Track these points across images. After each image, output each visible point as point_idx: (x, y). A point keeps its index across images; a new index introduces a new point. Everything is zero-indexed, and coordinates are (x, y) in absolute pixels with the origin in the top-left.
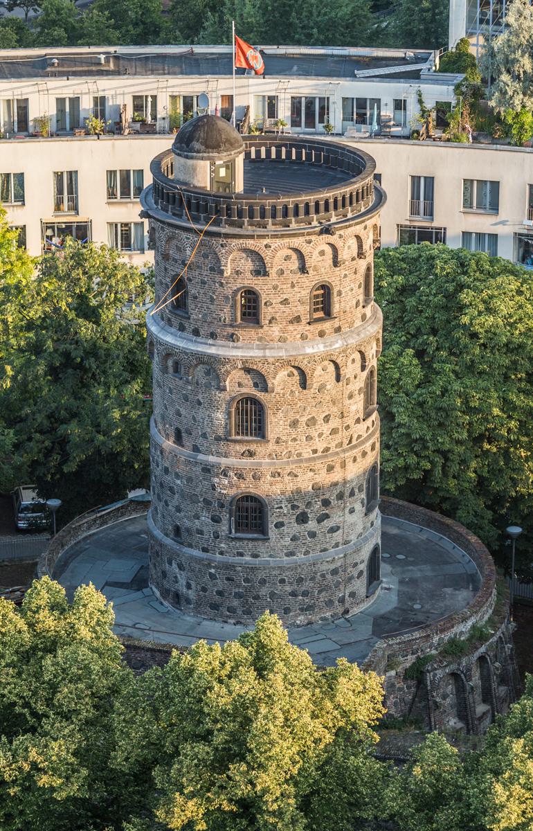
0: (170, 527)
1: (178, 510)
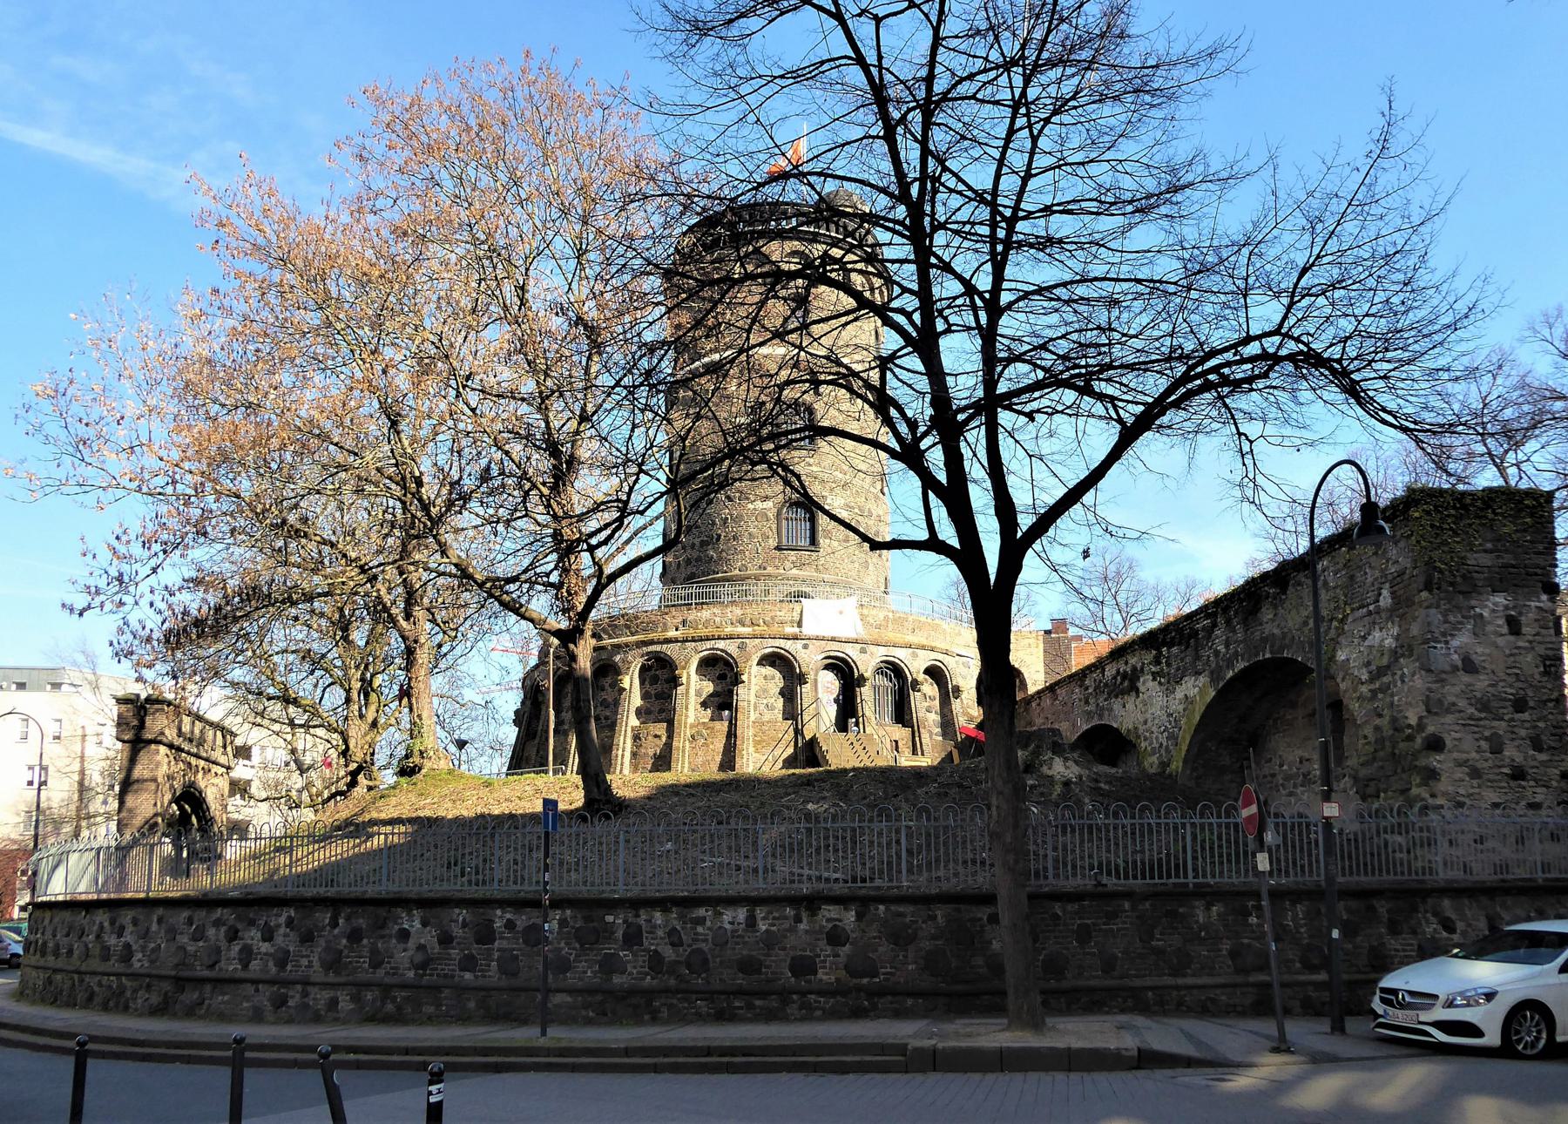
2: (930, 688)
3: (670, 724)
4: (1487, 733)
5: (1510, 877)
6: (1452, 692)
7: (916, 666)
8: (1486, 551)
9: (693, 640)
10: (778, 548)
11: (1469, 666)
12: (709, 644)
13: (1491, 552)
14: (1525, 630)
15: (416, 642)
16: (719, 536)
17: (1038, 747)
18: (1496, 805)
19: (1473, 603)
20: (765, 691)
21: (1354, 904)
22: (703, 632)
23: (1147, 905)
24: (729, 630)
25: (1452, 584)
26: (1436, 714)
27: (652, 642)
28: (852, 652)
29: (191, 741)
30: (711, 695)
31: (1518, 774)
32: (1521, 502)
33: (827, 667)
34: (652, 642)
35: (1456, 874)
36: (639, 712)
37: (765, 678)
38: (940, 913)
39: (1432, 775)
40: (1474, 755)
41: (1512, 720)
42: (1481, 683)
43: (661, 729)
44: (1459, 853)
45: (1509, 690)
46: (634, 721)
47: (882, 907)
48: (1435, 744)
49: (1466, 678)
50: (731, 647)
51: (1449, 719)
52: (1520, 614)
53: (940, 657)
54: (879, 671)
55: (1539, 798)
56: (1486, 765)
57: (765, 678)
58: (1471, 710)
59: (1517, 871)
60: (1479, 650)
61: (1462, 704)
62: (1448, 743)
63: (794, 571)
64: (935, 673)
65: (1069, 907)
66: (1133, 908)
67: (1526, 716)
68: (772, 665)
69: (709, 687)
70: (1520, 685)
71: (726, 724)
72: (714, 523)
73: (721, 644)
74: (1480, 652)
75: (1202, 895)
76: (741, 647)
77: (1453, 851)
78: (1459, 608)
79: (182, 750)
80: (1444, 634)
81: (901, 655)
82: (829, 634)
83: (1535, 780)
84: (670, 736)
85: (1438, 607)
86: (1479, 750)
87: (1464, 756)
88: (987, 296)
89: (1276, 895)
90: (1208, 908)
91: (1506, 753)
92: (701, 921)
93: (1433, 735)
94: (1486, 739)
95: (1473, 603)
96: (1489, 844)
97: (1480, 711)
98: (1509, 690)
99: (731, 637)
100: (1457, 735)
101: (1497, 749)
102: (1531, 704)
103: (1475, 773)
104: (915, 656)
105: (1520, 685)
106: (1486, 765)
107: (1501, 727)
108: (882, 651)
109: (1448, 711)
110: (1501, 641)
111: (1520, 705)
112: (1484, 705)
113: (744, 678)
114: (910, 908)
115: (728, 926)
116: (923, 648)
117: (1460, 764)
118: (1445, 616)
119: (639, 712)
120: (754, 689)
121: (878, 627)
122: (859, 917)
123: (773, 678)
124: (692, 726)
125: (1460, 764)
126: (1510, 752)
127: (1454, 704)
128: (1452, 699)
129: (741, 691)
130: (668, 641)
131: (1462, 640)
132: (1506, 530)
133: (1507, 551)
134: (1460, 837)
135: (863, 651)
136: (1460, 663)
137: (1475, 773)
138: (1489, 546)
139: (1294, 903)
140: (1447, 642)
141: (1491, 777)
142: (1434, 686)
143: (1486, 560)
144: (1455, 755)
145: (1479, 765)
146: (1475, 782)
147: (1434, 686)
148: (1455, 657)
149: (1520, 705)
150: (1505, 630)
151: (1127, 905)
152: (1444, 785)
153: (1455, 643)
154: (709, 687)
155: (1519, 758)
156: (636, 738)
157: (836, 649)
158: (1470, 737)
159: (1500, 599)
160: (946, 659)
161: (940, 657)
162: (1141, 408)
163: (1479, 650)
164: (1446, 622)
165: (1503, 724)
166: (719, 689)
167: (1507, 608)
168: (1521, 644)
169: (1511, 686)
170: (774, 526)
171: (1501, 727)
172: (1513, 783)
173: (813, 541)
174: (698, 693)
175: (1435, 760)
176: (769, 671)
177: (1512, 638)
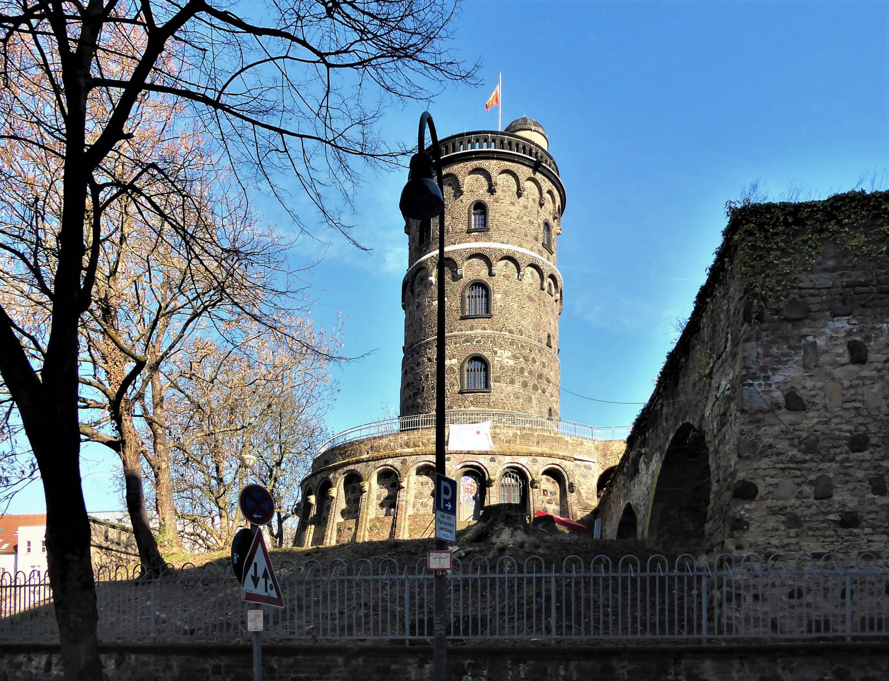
2: (548, 485)
3: (357, 518)
4: (812, 477)
5: (830, 634)
6: (768, 434)
7: (535, 468)
8: (825, 270)
9: (373, 460)
10: (461, 392)
11: (794, 402)
12: (382, 462)
13: (834, 270)
14: (872, 357)
15: (159, 469)
16: (423, 388)
17: (495, 520)
18: (817, 556)
19: (805, 331)
20: (421, 493)
21: (587, 664)
22: (383, 453)
23: (360, 660)
24: (399, 451)
25: (778, 312)
26: (748, 458)
27: (349, 464)
28: (484, 461)
29: (118, 544)
30: (386, 499)
31: (850, 520)
32: (877, 207)
33: (466, 474)
34: (349, 464)
35: (760, 633)
36: (343, 513)
37: (422, 484)
38: (176, 662)
39: (739, 525)
40: (793, 501)
41: (847, 460)
42: (810, 421)
43: (351, 523)
44: (767, 608)
45: (845, 427)
46: (339, 519)
47: (133, 657)
48: (746, 491)
49: (787, 417)
50: (396, 463)
51: (764, 463)
52: (868, 338)
53: (558, 461)
54: (506, 475)
55: (875, 547)
56: (808, 512)
57: (422, 484)
58: (795, 452)
59: (839, 627)
60: (809, 384)
61: (781, 445)
62: (762, 490)
63: (472, 408)
64: (554, 474)
65: (286, 661)
66: (347, 663)
67: (866, 454)
68: (427, 474)
69: (385, 493)
70: (860, 420)
71: (392, 518)
72: (421, 379)
73: (390, 462)
74: (808, 386)
75: (413, 653)
76: (404, 462)
77: (759, 607)
78: (785, 338)
79: (112, 550)
80: (764, 369)
81: (523, 461)
82: (465, 449)
83: (873, 527)
84: (356, 529)
85: (758, 339)
86: (800, 496)
87: (780, 503)
88: (79, 15)
89: (268, 651)
90: (421, 665)
91: (836, 498)
92: (19, 666)
93: (744, 481)
94: (811, 483)
95: (805, 331)
96: (808, 598)
97: (805, 452)
98: (845, 427)
99: (396, 456)
100: (774, 481)
101: (824, 493)
102: (874, 441)
103: (794, 521)
104: (535, 461)
105: (860, 420)
106: (808, 512)
107: (831, 469)
108: (508, 459)
109: (763, 454)
110: (838, 373)
111: (858, 443)
112: (810, 446)
113: (404, 484)
114: (153, 658)
115: (33, 671)
116: (542, 455)
117: (773, 512)
118: (767, 347)
119: (343, 513)
120: (412, 492)
121: (509, 442)
122: (118, 664)
123: (427, 483)
124: (371, 520)
125: (773, 512)
126: (843, 497)
127: (770, 446)
128: (767, 440)
129: (401, 493)
130: (358, 462)
131: (790, 373)
132: (854, 242)
133: (854, 267)
134: (769, 592)
135: (493, 460)
136: (782, 400)
137: (794, 521)
138: (831, 263)
139: (516, 662)
140: (767, 378)
141: (814, 525)
142: (746, 428)
143: (825, 280)
144: (769, 502)
145: (798, 512)
146: (792, 532)
147: (746, 428)
148: (779, 393)
149: (858, 443)
150: (846, 358)
151: (340, 660)
152: (753, 535)
153: (778, 378)
154: (385, 493)
155: (852, 503)
156: (339, 530)
157: (472, 460)
158: (789, 482)
159: (842, 324)
160: (565, 463)
161: (558, 461)
162: (99, 76)
163: (809, 384)
164: (767, 355)
165: (834, 465)
166: (391, 494)
167: (849, 333)
168: (865, 373)
169: (848, 422)
170: (458, 377)
171: (831, 469)
172: (842, 531)
173: (487, 385)
174: (378, 498)
175: (742, 509)
176: (425, 478)
177: (854, 368)
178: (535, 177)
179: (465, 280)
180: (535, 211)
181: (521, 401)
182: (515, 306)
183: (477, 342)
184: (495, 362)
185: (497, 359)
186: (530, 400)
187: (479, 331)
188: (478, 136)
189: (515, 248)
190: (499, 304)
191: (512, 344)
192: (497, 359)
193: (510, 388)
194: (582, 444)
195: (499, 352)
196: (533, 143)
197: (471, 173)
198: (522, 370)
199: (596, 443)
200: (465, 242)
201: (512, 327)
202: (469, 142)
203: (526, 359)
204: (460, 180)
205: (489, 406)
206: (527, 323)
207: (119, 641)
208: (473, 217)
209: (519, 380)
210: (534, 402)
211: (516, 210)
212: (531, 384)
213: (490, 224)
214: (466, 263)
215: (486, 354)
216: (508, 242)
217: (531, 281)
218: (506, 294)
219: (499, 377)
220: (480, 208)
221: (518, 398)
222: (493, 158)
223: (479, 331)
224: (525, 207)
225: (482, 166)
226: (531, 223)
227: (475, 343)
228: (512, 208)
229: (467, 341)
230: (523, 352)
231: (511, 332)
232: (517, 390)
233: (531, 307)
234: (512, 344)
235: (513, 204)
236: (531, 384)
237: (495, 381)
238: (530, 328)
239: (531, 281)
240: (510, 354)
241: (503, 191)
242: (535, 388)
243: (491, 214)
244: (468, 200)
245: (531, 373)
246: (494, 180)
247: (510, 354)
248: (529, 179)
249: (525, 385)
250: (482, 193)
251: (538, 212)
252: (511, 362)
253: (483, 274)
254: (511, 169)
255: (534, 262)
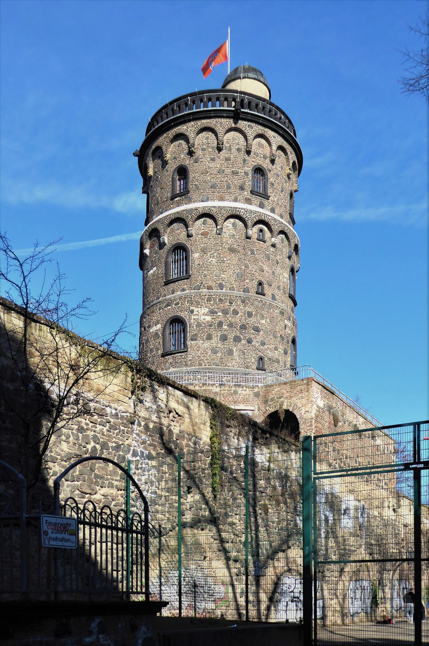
0: (253, 360)
1: (263, 344)
10: (163, 356)
178: (238, 126)
179: (168, 246)
180: (240, 160)
181: (219, 355)
182: (214, 261)
183: (176, 305)
184: (192, 321)
185: (193, 317)
186: (230, 352)
187: (179, 293)
188: (197, 96)
189: (209, 204)
190: (197, 263)
191: (209, 300)
192: (193, 317)
193: (207, 344)
194: (236, 392)
195: (196, 310)
196: (236, 92)
197: (172, 141)
198: (220, 324)
199: (256, 390)
200: (170, 209)
201: (210, 283)
202: (202, 101)
203: (225, 312)
204: (164, 150)
205: (186, 365)
206: (229, 276)
207: (166, 600)
208: (178, 182)
209: (216, 335)
210: (236, 354)
211: (216, 165)
212: (231, 336)
213: (191, 186)
214: (169, 230)
215: (183, 315)
216: (207, 200)
217: (233, 232)
218: (204, 251)
219: (196, 334)
220: (182, 172)
221: (215, 352)
222: (189, 121)
223: (179, 293)
224: (228, 159)
225: (181, 131)
226: (235, 173)
227: (174, 306)
228: (212, 165)
229: (168, 305)
230: (222, 306)
231: (209, 288)
232: (214, 345)
233: (232, 259)
234: (209, 300)
235: (213, 160)
236: (231, 336)
237: (192, 340)
238: (232, 280)
239: (233, 232)
240: (207, 310)
241: (203, 150)
242: (237, 339)
243: (191, 175)
244: (172, 167)
245: (231, 325)
246: (191, 141)
247: (207, 310)
248: (230, 130)
249: (224, 338)
250: (184, 159)
251: (244, 161)
252: (208, 318)
253: (182, 237)
254: (209, 125)
255: (234, 213)
